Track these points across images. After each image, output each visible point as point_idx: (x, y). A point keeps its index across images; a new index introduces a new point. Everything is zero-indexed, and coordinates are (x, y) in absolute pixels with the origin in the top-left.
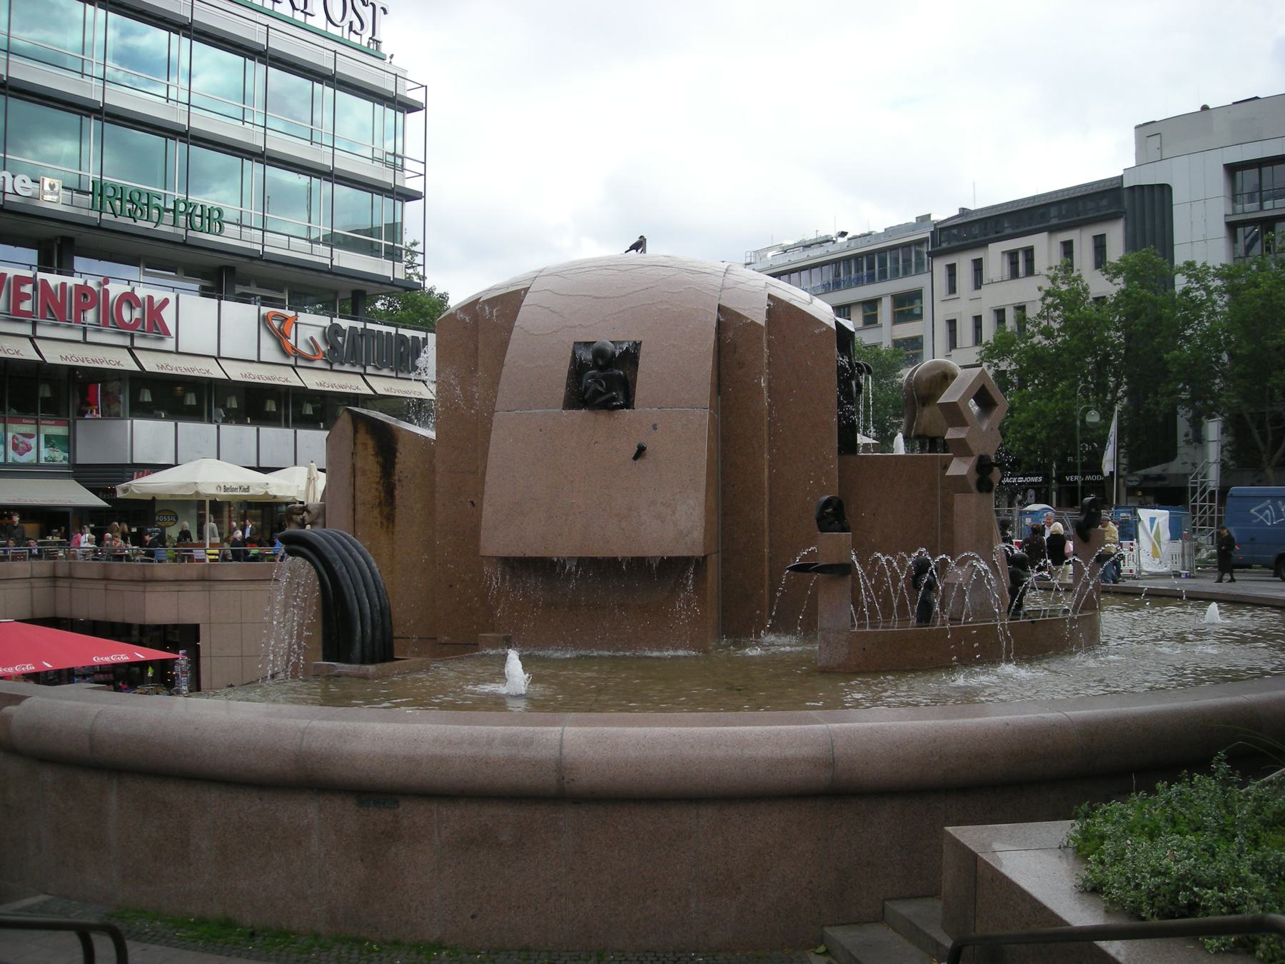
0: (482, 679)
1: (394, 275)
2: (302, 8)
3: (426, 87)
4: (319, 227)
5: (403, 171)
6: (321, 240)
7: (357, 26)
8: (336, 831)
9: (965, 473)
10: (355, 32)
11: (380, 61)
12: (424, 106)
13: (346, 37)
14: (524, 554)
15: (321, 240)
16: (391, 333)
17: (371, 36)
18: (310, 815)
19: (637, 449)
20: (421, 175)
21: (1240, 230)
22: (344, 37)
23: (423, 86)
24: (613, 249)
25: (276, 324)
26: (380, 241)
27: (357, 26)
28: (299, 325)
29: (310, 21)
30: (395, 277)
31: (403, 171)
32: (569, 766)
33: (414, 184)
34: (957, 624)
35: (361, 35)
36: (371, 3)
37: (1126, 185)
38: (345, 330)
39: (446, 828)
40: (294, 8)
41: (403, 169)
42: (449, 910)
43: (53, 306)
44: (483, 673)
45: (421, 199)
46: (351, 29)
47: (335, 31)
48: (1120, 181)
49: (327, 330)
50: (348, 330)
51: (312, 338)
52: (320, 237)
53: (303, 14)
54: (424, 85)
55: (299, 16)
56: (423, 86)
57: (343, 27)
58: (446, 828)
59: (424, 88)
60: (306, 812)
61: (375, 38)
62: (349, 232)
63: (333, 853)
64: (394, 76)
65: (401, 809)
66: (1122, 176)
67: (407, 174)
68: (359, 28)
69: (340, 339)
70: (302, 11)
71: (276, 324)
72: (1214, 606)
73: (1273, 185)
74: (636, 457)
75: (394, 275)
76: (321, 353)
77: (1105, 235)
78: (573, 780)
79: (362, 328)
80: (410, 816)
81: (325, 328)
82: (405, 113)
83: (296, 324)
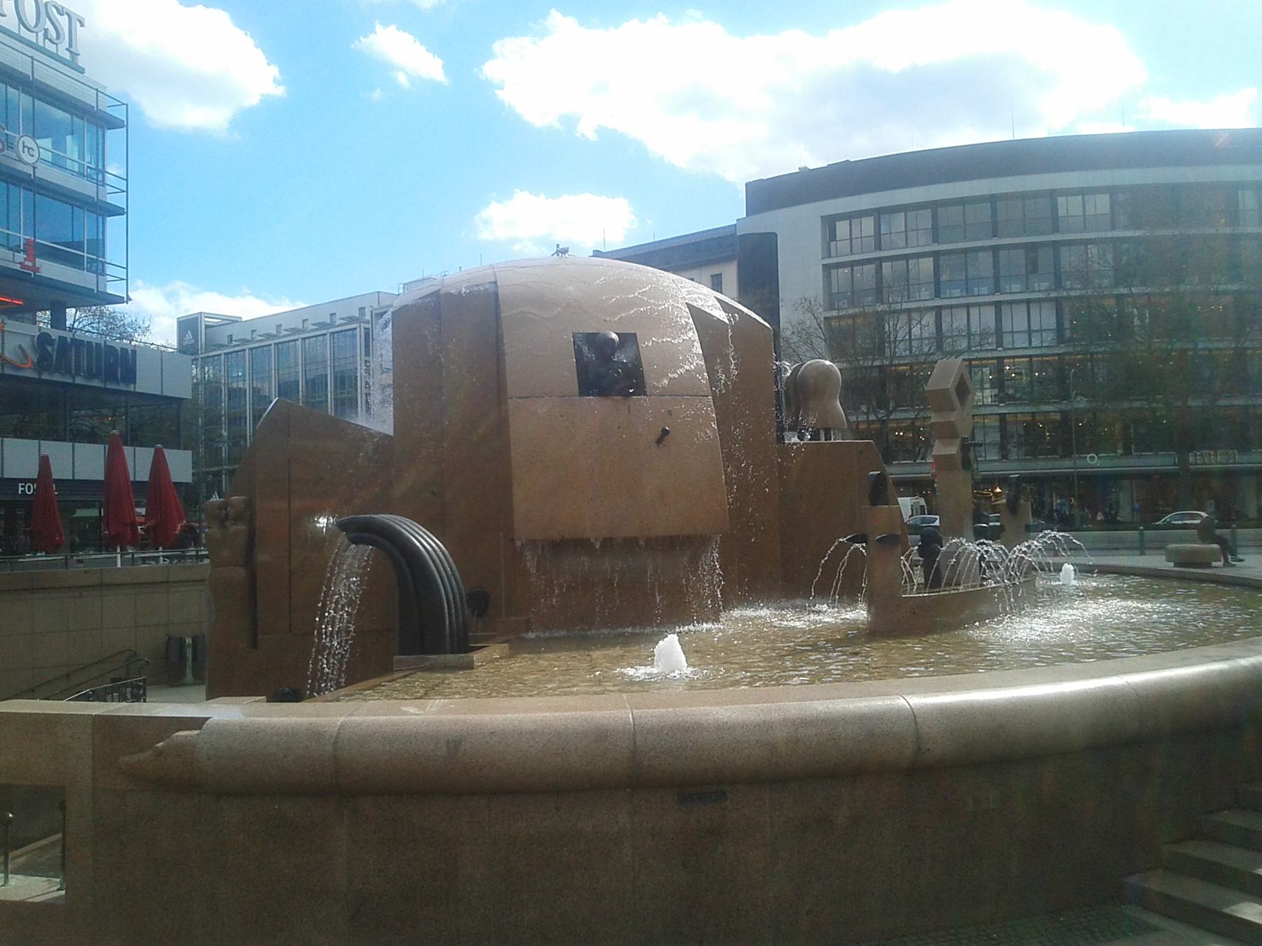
3: (127, 105)
4: (19, 235)
5: (104, 187)
6: (22, 248)
7: (53, 33)
8: (653, 836)
10: (50, 40)
12: (125, 124)
15: (22, 248)
16: (100, 344)
20: (123, 191)
21: (834, 272)
22: (39, 44)
23: (123, 104)
26: (82, 253)
27: (53, 33)
28: (6, 334)
31: (104, 187)
32: (926, 736)
35: (57, 44)
37: (738, 234)
41: (104, 184)
43: (75, 254)
44: (1150, 631)
45: (123, 215)
47: (31, 37)
48: (733, 228)
51: (20, 347)
52: (20, 246)
54: (125, 103)
56: (123, 104)
59: (125, 106)
61: (71, 49)
66: (735, 225)
67: (109, 189)
68: (55, 36)
69: (49, 348)
73: (917, 234)
75: (97, 288)
77: (721, 274)
78: (928, 750)
80: (739, 807)
81: (34, 336)
82: (106, 128)
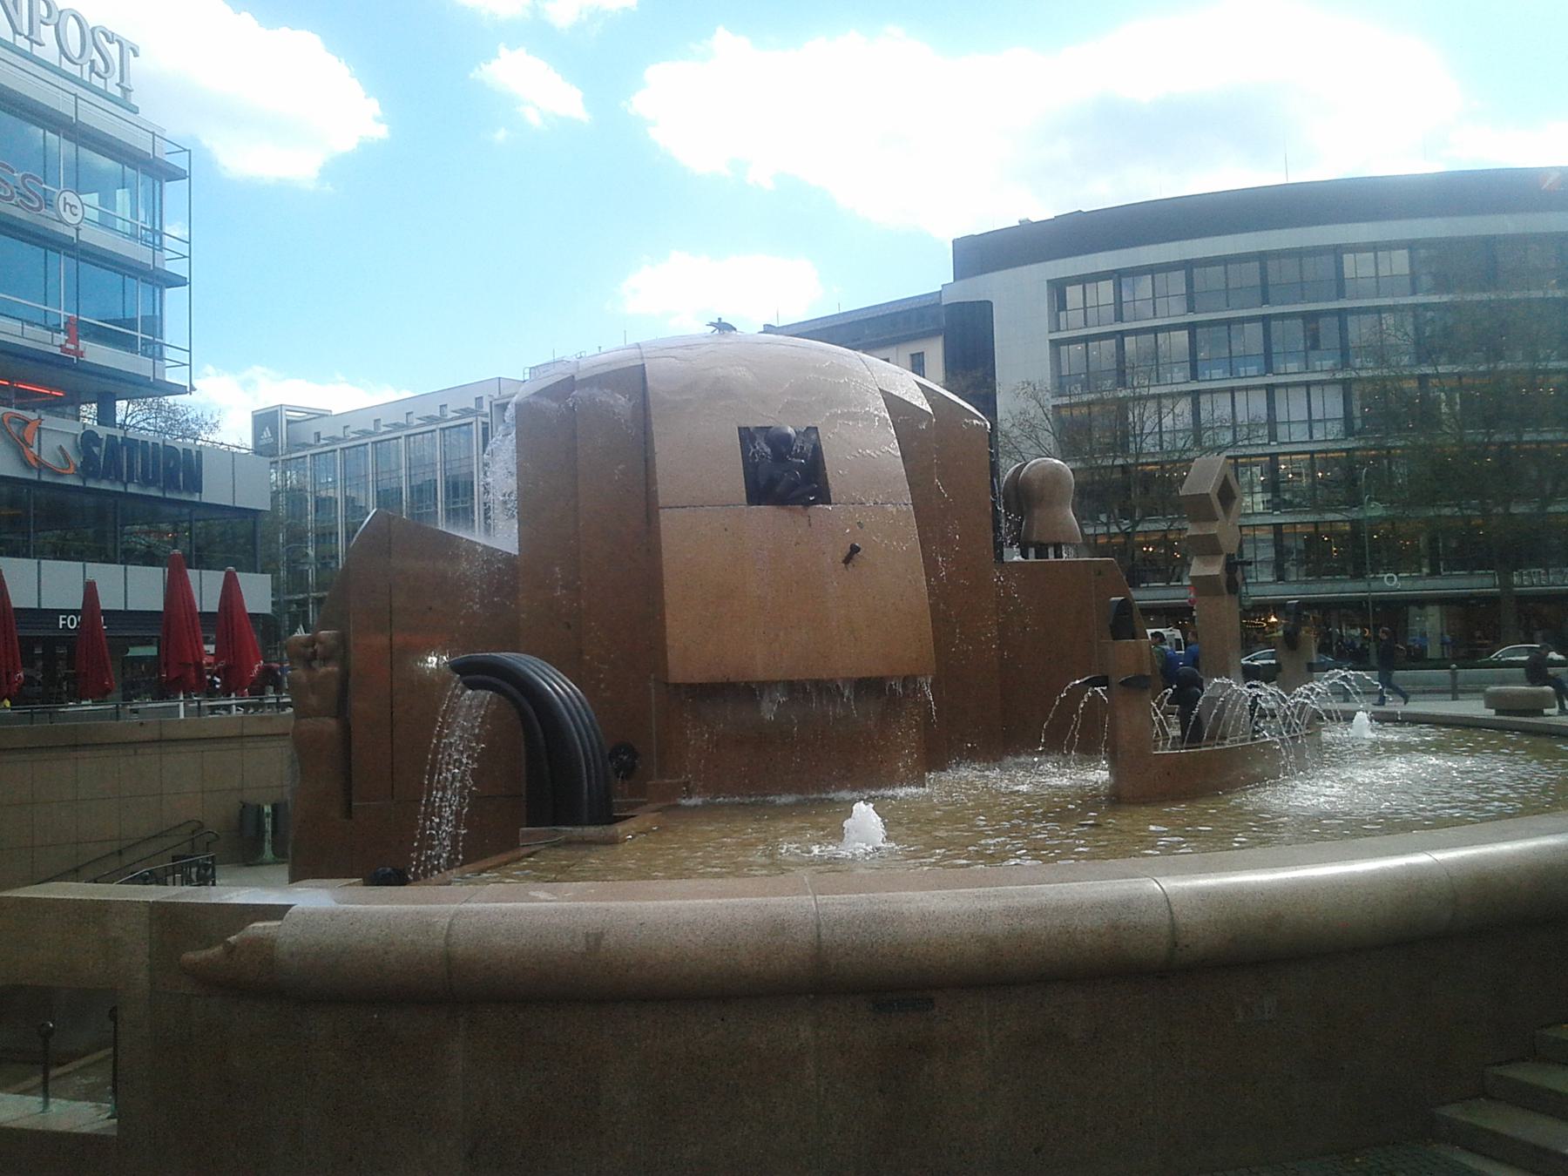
0: (746, 842)
1: (154, 376)
2: (26, 33)
3: (190, 151)
9: (1217, 573)
11: (132, 114)
13: (86, 78)
14: (728, 679)
15: (62, 327)
16: (157, 444)
17: (118, 81)
18: (802, 1036)
19: (849, 550)
20: (185, 257)
22: (85, 78)
23: (185, 150)
24: (696, 327)
25: (14, 428)
26: (135, 334)
27: (101, 65)
29: (37, 51)
30: (157, 377)
33: (177, 268)
34: (1196, 747)
35: (105, 79)
36: (117, 41)
38: (102, 439)
39: (1000, 1029)
40: (15, 31)
42: (1006, 1145)
46: (92, 69)
49: (79, 438)
50: (105, 439)
53: (28, 42)
54: (188, 148)
55: (23, 43)
56: (185, 150)
57: (82, 65)
58: (1000, 1029)
59: (187, 152)
60: (798, 1030)
62: (99, 321)
63: (838, 1086)
64: (151, 135)
65: (937, 1009)
67: (168, 255)
68: (103, 70)
70: (26, 37)
71: (14, 428)
72: (1179, 733)
74: (847, 560)
76: (72, 467)
78: (1187, 946)
79: (122, 438)
81: (77, 435)
83: (39, 429)
